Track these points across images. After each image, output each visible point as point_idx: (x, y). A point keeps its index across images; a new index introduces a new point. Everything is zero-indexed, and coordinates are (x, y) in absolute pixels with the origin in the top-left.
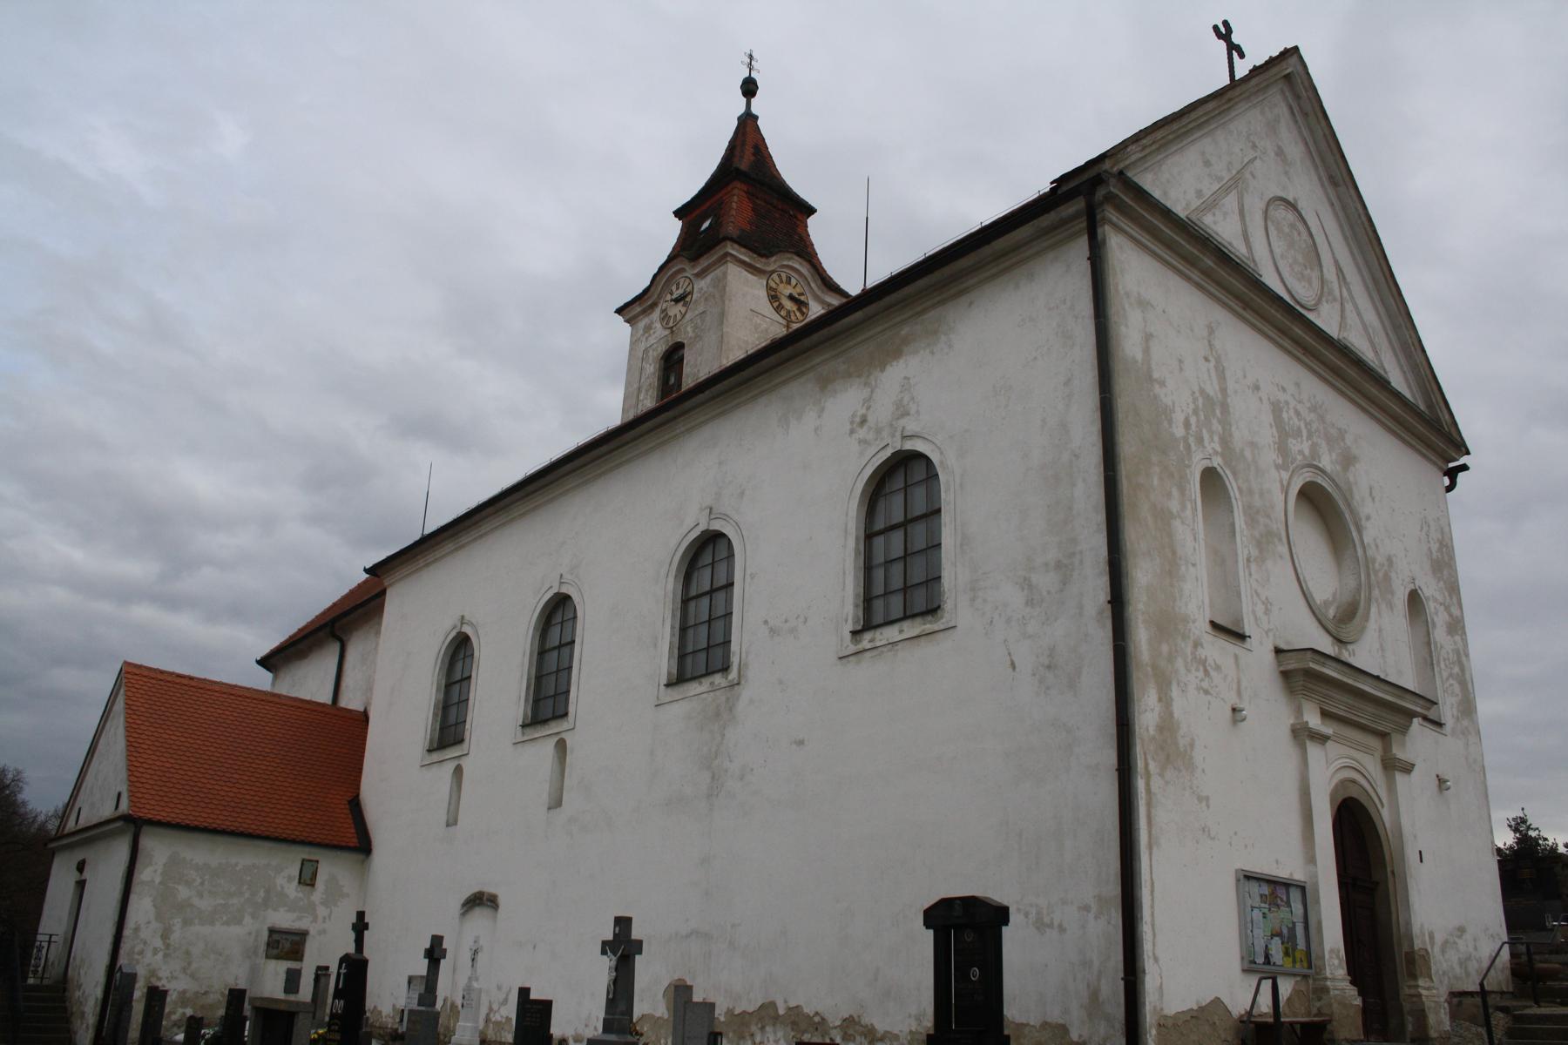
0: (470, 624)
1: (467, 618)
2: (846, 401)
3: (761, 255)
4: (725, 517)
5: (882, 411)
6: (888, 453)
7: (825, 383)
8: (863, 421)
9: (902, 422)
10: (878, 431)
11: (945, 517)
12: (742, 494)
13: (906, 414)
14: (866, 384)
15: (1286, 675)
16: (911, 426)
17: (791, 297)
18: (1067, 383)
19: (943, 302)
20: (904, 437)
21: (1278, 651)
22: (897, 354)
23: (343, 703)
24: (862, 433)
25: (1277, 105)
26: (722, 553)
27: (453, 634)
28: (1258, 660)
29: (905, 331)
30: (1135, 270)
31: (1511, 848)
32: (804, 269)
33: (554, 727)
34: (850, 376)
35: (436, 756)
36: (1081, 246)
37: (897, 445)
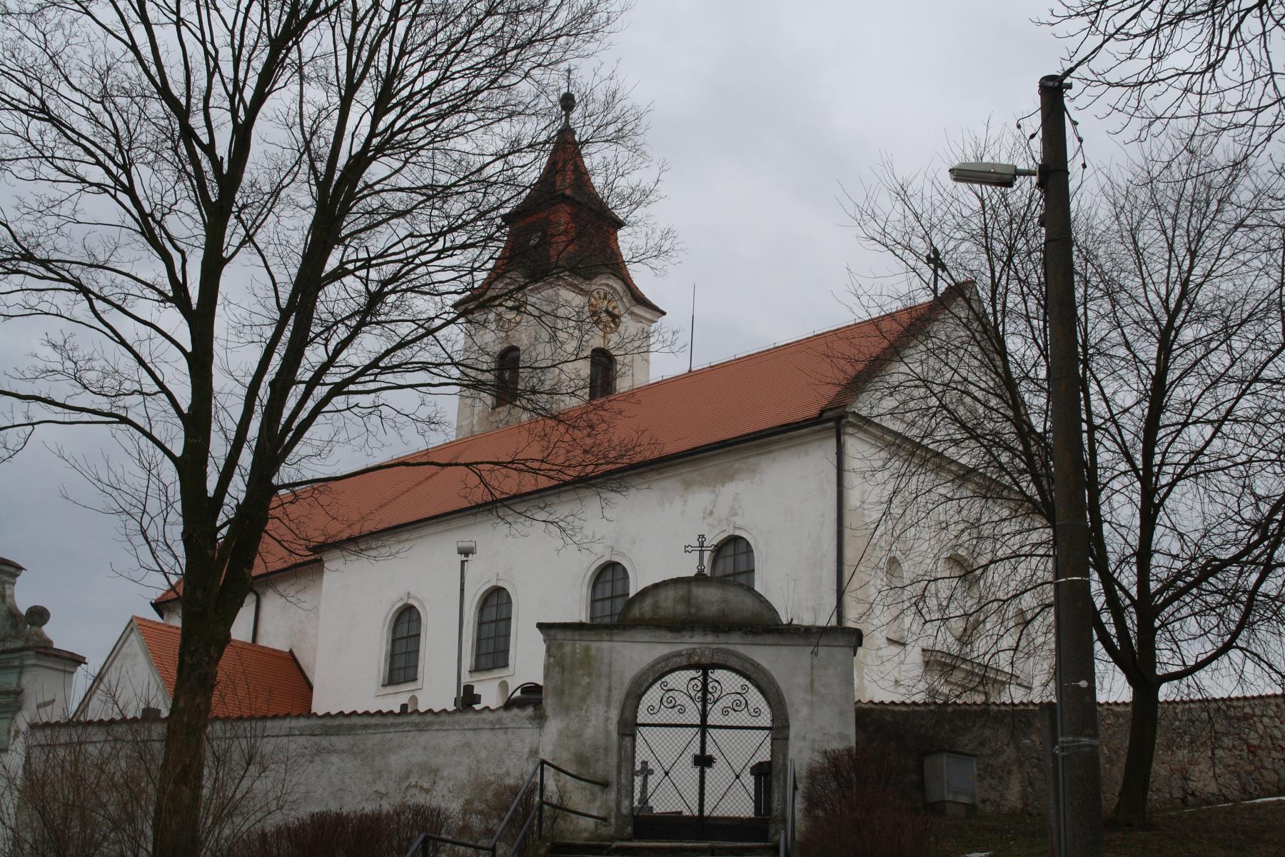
0: (415, 598)
1: (412, 593)
2: (700, 499)
3: (586, 279)
4: (622, 554)
5: (722, 510)
6: (725, 535)
7: (688, 485)
8: (711, 513)
9: (734, 518)
10: (720, 521)
11: (757, 575)
12: (634, 542)
13: (736, 514)
14: (713, 492)
15: (927, 663)
16: (739, 522)
17: (607, 311)
18: (822, 516)
19: (759, 455)
20: (735, 528)
21: (924, 650)
22: (731, 477)
23: (263, 641)
24: (710, 520)
25: (854, 639)
26: (619, 575)
27: (400, 604)
28: (914, 656)
29: (737, 465)
30: (859, 450)
31: (849, 750)
32: (618, 285)
33: (497, 673)
34: (703, 484)
35: (390, 689)
36: (833, 442)
37: (730, 532)
